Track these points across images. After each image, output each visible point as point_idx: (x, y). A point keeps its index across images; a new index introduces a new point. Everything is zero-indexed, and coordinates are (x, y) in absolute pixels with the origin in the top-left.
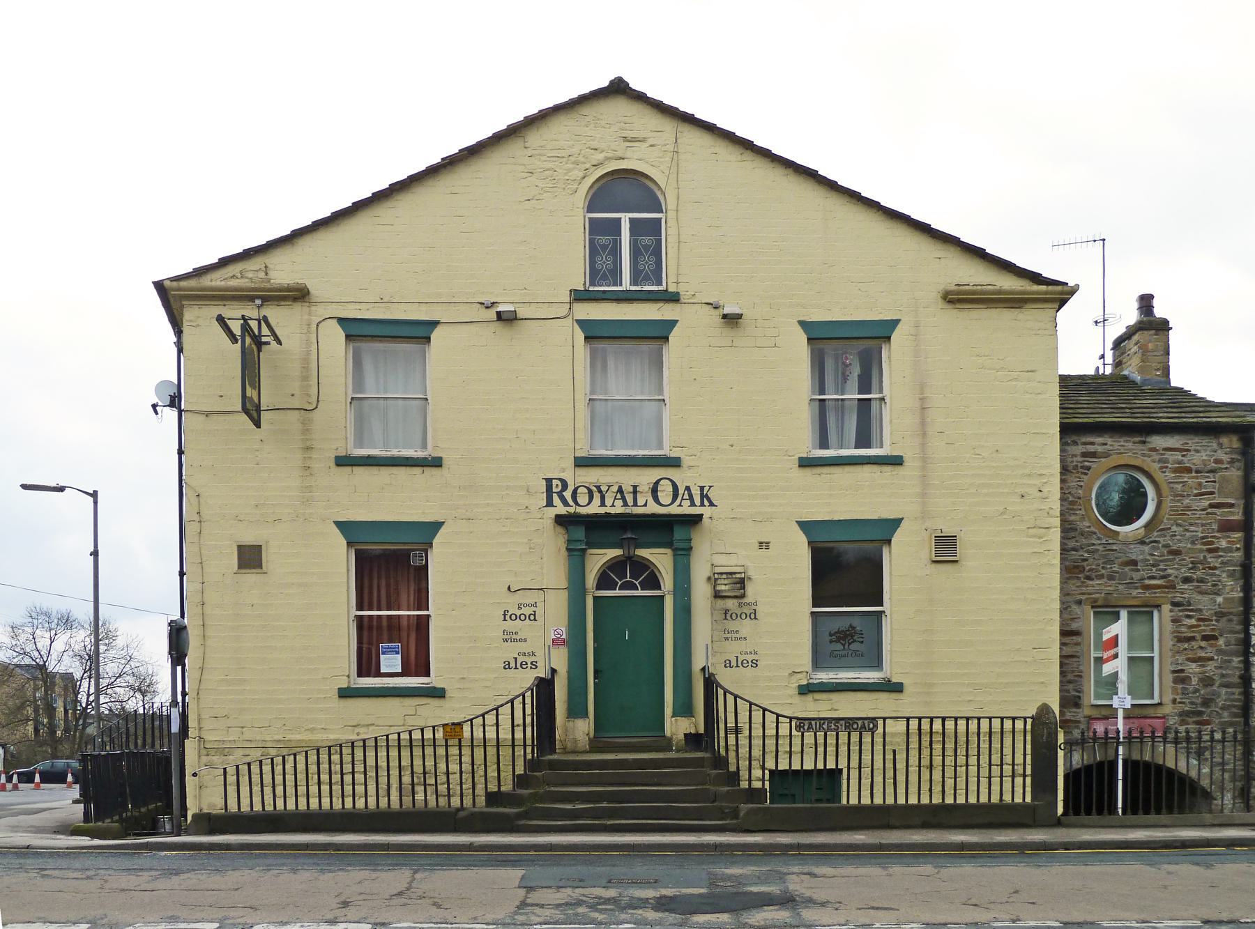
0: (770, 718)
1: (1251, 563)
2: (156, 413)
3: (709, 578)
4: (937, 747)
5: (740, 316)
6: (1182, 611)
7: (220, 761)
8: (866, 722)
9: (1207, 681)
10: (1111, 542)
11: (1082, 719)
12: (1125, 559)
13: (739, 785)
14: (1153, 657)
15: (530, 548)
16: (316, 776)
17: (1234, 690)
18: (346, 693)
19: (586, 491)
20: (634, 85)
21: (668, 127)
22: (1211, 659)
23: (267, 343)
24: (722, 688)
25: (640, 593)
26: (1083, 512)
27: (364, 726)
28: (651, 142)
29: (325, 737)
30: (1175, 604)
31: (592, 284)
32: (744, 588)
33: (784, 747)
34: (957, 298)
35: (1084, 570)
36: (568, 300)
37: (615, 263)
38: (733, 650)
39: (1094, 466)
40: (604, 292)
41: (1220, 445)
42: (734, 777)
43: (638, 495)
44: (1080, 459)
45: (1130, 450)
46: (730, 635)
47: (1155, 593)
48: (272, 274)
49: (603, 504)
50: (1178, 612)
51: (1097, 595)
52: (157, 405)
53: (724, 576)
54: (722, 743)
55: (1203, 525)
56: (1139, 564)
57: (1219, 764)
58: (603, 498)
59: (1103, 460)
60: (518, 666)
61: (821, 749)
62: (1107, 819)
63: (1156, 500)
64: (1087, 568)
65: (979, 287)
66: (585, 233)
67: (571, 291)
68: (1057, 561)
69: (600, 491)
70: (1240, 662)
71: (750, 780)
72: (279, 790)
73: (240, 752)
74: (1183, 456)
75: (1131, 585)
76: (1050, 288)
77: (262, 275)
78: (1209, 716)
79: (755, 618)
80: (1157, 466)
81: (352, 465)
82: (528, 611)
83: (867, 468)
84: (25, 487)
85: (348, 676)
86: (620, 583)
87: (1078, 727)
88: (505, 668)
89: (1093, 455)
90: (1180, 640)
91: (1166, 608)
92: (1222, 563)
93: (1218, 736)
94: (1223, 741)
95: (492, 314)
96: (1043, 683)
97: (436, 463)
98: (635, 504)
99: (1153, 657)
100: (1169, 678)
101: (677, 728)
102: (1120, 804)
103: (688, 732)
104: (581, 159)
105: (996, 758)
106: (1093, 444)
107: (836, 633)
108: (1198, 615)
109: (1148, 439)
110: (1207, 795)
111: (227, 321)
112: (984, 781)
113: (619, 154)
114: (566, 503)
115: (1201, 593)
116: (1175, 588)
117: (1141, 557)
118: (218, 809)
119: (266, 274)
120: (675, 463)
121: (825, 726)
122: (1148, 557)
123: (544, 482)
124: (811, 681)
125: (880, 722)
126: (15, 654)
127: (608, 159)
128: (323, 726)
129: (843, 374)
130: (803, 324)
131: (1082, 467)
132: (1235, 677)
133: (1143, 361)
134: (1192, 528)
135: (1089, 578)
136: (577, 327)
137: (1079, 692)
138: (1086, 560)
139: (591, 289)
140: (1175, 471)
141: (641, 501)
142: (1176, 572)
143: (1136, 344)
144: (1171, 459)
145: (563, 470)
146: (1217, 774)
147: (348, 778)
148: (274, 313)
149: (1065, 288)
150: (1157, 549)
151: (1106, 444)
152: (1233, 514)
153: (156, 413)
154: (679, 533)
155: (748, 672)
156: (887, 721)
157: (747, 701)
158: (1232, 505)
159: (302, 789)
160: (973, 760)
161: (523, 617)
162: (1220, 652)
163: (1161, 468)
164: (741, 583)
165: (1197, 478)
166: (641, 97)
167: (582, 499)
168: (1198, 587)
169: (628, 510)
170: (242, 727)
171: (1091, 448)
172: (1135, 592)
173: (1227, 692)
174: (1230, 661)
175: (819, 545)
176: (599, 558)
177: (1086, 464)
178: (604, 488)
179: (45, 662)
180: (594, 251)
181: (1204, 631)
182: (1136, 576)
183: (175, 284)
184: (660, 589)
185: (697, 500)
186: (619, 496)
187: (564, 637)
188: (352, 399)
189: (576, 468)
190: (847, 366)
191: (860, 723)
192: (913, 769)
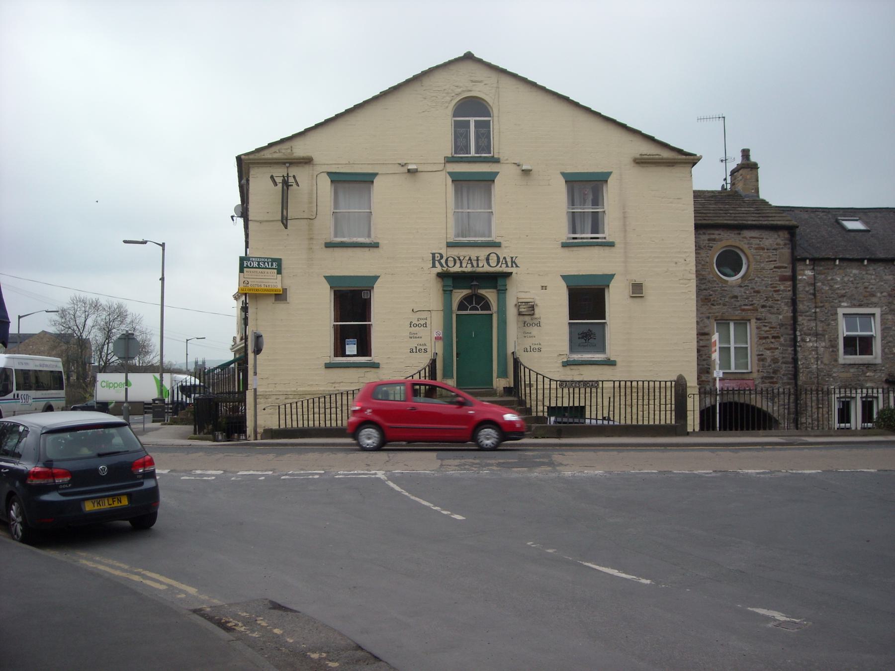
0: (547, 381)
1: (796, 298)
2: (233, 220)
3: (516, 305)
4: (635, 395)
5: (531, 170)
6: (761, 323)
7: (264, 402)
8: (593, 383)
9: (775, 361)
10: (724, 285)
11: (711, 380)
12: (731, 295)
13: (531, 414)
14: (747, 348)
15: (424, 289)
16: (312, 410)
17: (789, 365)
18: (329, 366)
19: (452, 259)
20: (477, 55)
21: (493, 77)
22: (777, 348)
23: (292, 185)
24: (523, 365)
25: (480, 312)
26: (709, 270)
27: (337, 383)
28: (486, 82)
29: (317, 389)
30: (758, 319)
31: (455, 153)
32: (534, 310)
33: (553, 395)
34: (641, 162)
35: (710, 300)
36: (444, 162)
37: (467, 141)
38: (528, 343)
39: (714, 246)
40: (461, 157)
41: (779, 236)
42: (529, 411)
43: (479, 262)
44: (708, 242)
45: (733, 238)
46: (526, 335)
47: (747, 313)
48: (294, 150)
49: (461, 266)
50: (759, 323)
51: (717, 314)
52: (234, 216)
53: (524, 304)
54: (523, 392)
55: (771, 278)
56: (739, 298)
57: (782, 405)
58: (461, 263)
59: (719, 243)
60: (417, 351)
61: (572, 396)
62: (711, 432)
63: (747, 264)
64: (712, 300)
65: (652, 157)
66: (452, 128)
67: (445, 157)
68: (694, 297)
69: (460, 260)
70: (792, 350)
71: (537, 412)
72: (294, 417)
73: (275, 397)
74: (760, 241)
75: (735, 308)
76: (687, 157)
77: (289, 151)
78: (777, 379)
79: (540, 326)
80: (746, 246)
81: (333, 247)
82: (422, 322)
83: (597, 248)
84: (125, 242)
85: (330, 357)
86: (470, 307)
87: (708, 384)
88: (410, 352)
89: (714, 240)
90: (761, 338)
91: (753, 321)
92: (781, 298)
93: (781, 390)
94: (784, 393)
95: (405, 169)
96: (688, 361)
97: (376, 246)
98: (478, 266)
99: (747, 348)
100: (755, 358)
101: (500, 384)
102: (718, 425)
103: (505, 386)
104: (450, 91)
105: (663, 401)
106: (713, 234)
107: (582, 333)
108: (770, 326)
109: (742, 232)
110: (777, 422)
111: (275, 178)
112: (657, 412)
113: (469, 88)
114: (442, 266)
115: (771, 313)
116: (757, 310)
117: (740, 294)
118: (275, 426)
119: (291, 151)
120: (498, 245)
121: (574, 385)
122: (743, 294)
123: (431, 255)
124: (569, 359)
125: (601, 383)
126: (63, 328)
127: (463, 91)
128: (317, 383)
129: (584, 199)
130: (563, 174)
131: (708, 246)
132: (789, 357)
133: (744, 185)
134: (766, 279)
135: (713, 305)
136: (448, 175)
137: (709, 365)
138: (711, 295)
139: (455, 156)
140: (756, 249)
141: (481, 265)
142: (757, 302)
143: (741, 175)
144: (754, 242)
145: (441, 249)
146: (781, 411)
147: (328, 411)
148: (293, 171)
149: (695, 157)
150: (748, 290)
151: (720, 234)
152: (786, 272)
153: (233, 220)
154: (500, 282)
155: (536, 354)
156: (604, 382)
157: (535, 372)
158: (786, 268)
159: (306, 417)
160: (652, 402)
161: (420, 325)
162: (781, 345)
163: (749, 247)
164: (532, 308)
165: (767, 253)
166: (480, 61)
167: (451, 264)
168: (770, 310)
169: (474, 269)
170: (276, 384)
171: (713, 237)
172: (737, 313)
173: (785, 367)
174: (787, 350)
175: (571, 287)
176: (459, 295)
177: (711, 245)
178: (462, 258)
179: (81, 334)
180: (457, 136)
181: (773, 333)
182: (738, 304)
183: (247, 157)
184: (490, 310)
185: (510, 264)
186: (469, 262)
187: (441, 336)
188: (333, 212)
189: (448, 248)
190: (586, 195)
191: (591, 383)
192: (623, 406)
